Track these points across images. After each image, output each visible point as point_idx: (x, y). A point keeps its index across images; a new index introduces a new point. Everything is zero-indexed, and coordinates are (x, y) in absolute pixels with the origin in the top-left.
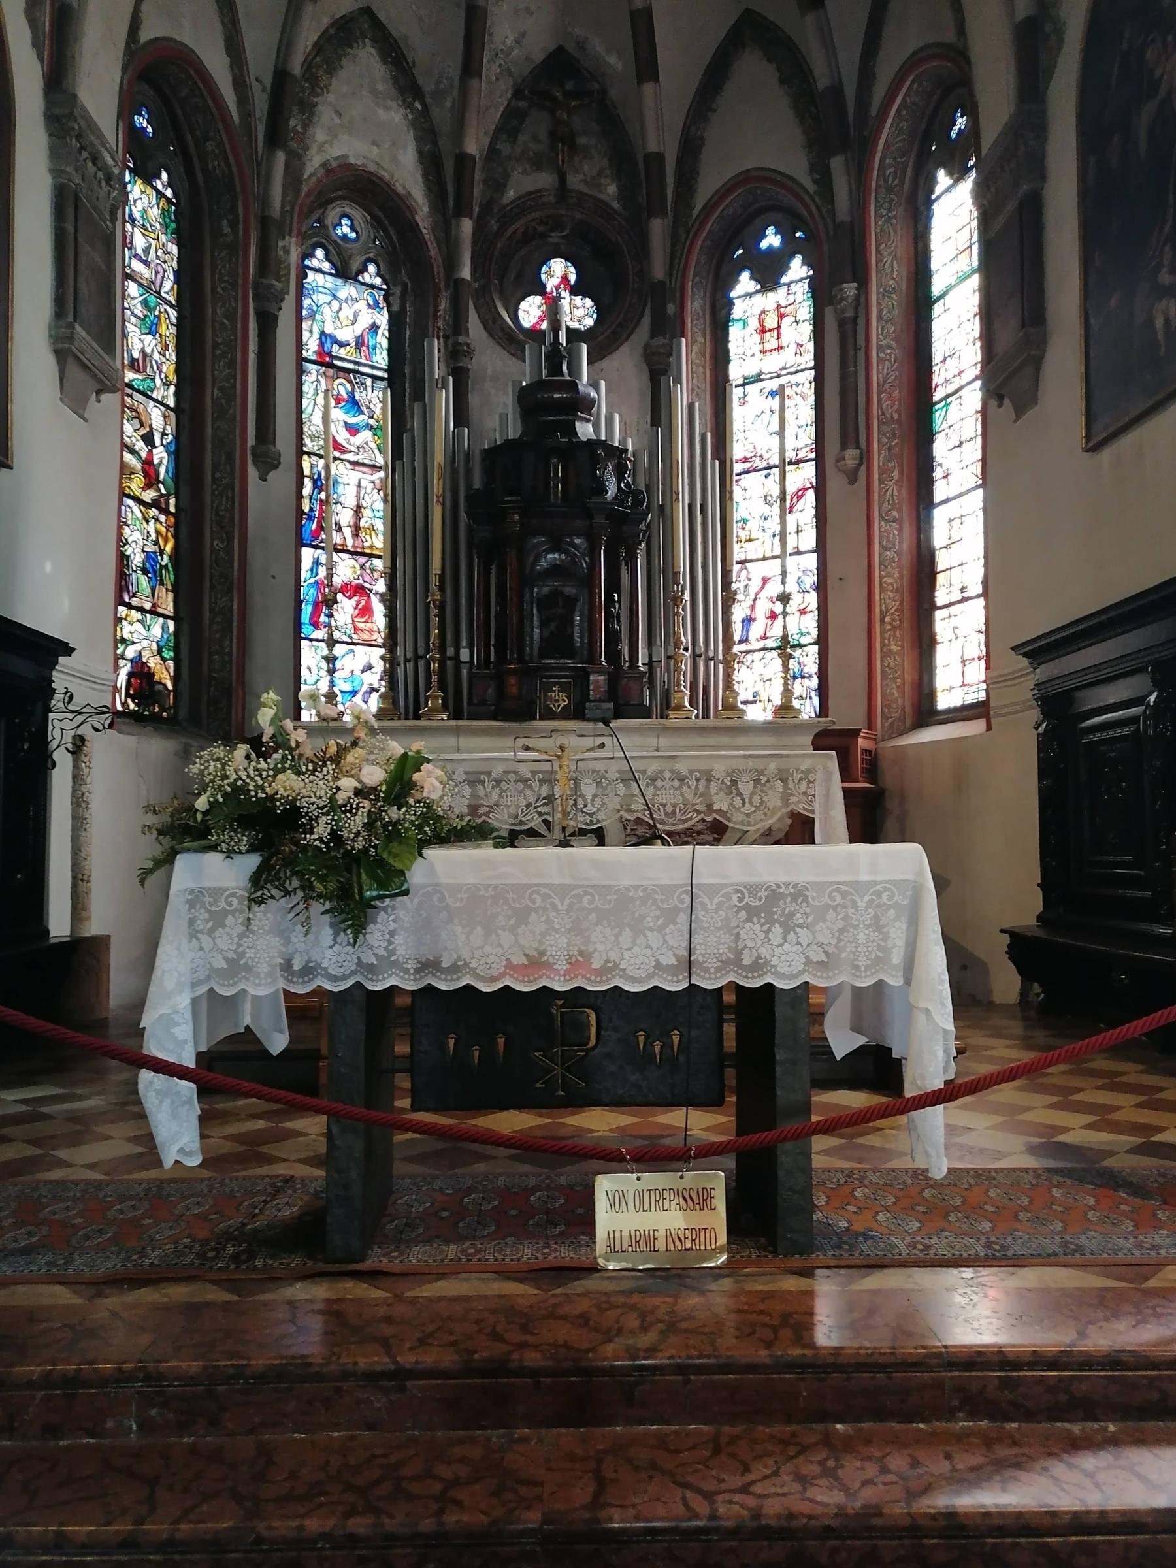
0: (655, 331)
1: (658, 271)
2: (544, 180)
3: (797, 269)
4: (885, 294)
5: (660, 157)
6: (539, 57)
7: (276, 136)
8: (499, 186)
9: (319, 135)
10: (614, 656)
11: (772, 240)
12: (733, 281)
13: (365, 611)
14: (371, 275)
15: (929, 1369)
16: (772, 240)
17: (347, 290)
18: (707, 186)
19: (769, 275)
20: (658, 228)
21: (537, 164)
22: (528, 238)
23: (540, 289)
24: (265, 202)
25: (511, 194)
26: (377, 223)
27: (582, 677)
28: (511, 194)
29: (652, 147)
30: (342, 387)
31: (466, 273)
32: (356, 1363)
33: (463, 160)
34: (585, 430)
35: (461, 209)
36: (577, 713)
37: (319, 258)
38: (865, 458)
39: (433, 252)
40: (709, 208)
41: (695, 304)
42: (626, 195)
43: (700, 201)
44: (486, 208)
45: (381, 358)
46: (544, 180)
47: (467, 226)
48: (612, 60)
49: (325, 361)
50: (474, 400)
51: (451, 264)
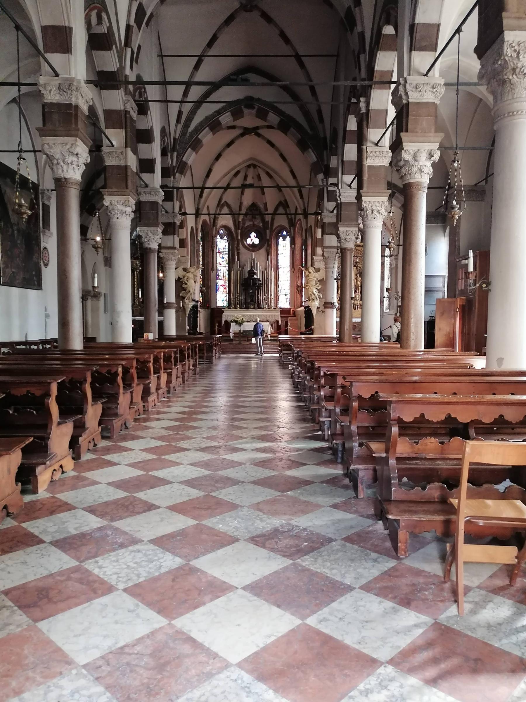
0: (268, 246)
1: (268, 237)
2: (251, 223)
3: (288, 238)
4: (297, 247)
5: (268, 221)
6: (250, 204)
7: (214, 225)
8: (244, 224)
9: (219, 221)
10: (258, 302)
11: (285, 233)
12: (279, 238)
13: (225, 288)
14: (225, 238)
15: (424, 511)
16: (285, 233)
17: (222, 241)
18: (275, 226)
19: (284, 239)
20: (268, 231)
21: (250, 220)
22: (249, 230)
23: (250, 237)
24: (213, 234)
25: (246, 225)
26: (226, 230)
27: (255, 304)
28: (246, 225)
29: (267, 220)
30: (221, 255)
31: (239, 238)
32: (138, 576)
33: (239, 222)
34: (255, 276)
35: (239, 229)
36: (254, 308)
37: (218, 237)
38: (295, 270)
39: (235, 235)
40: (275, 229)
41: (273, 243)
42: (263, 225)
43: (274, 227)
44: (242, 227)
45: (227, 250)
46: (251, 223)
47: (240, 231)
48: (261, 206)
49: (219, 252)
50: (240, 256)
51: (237, 236)
